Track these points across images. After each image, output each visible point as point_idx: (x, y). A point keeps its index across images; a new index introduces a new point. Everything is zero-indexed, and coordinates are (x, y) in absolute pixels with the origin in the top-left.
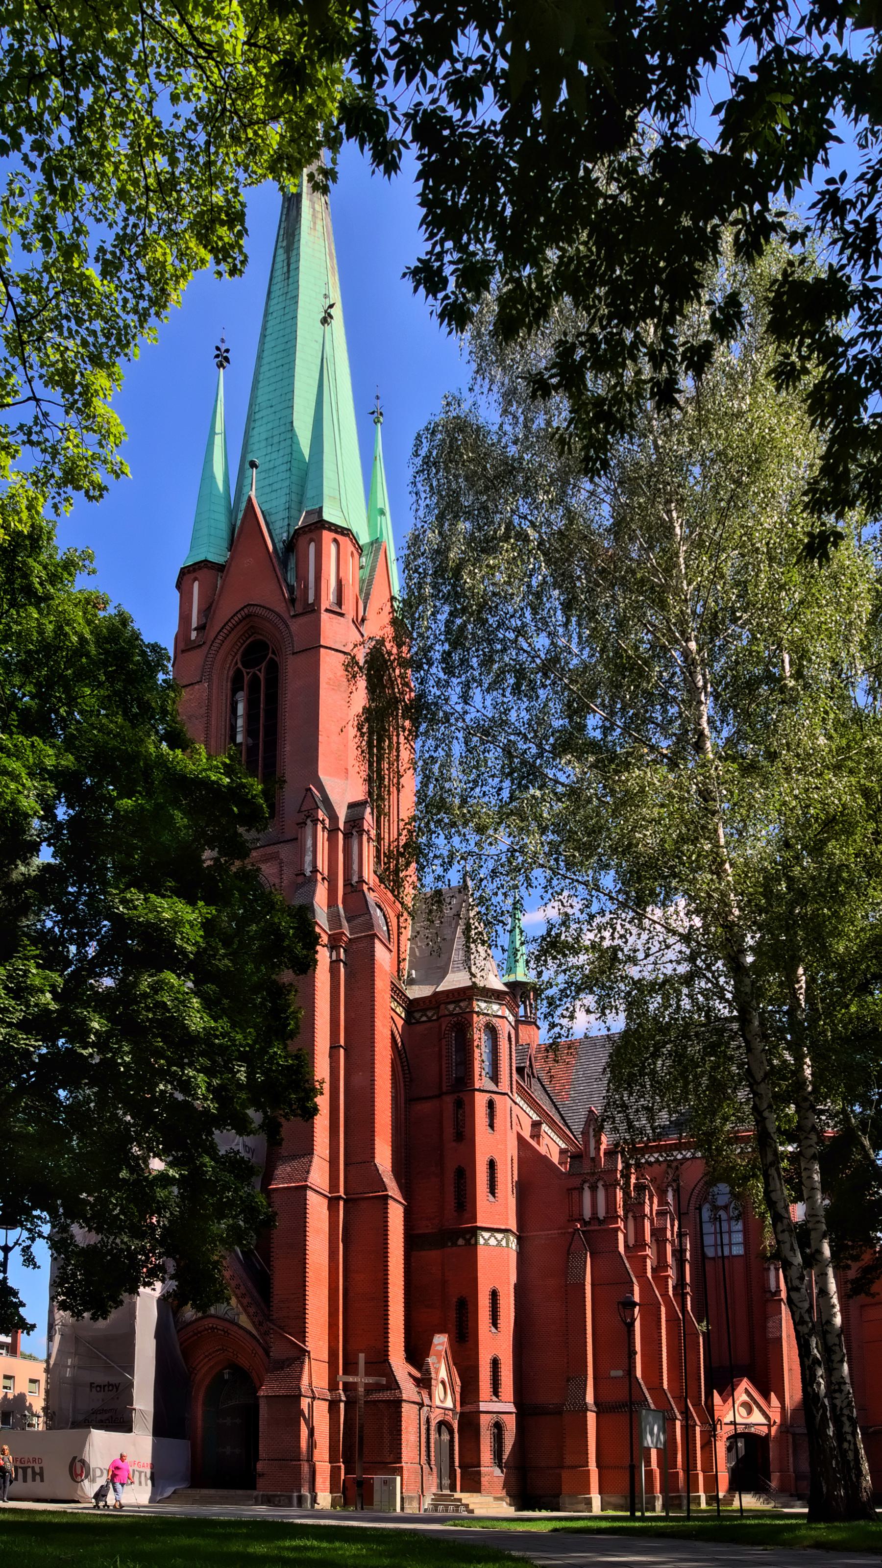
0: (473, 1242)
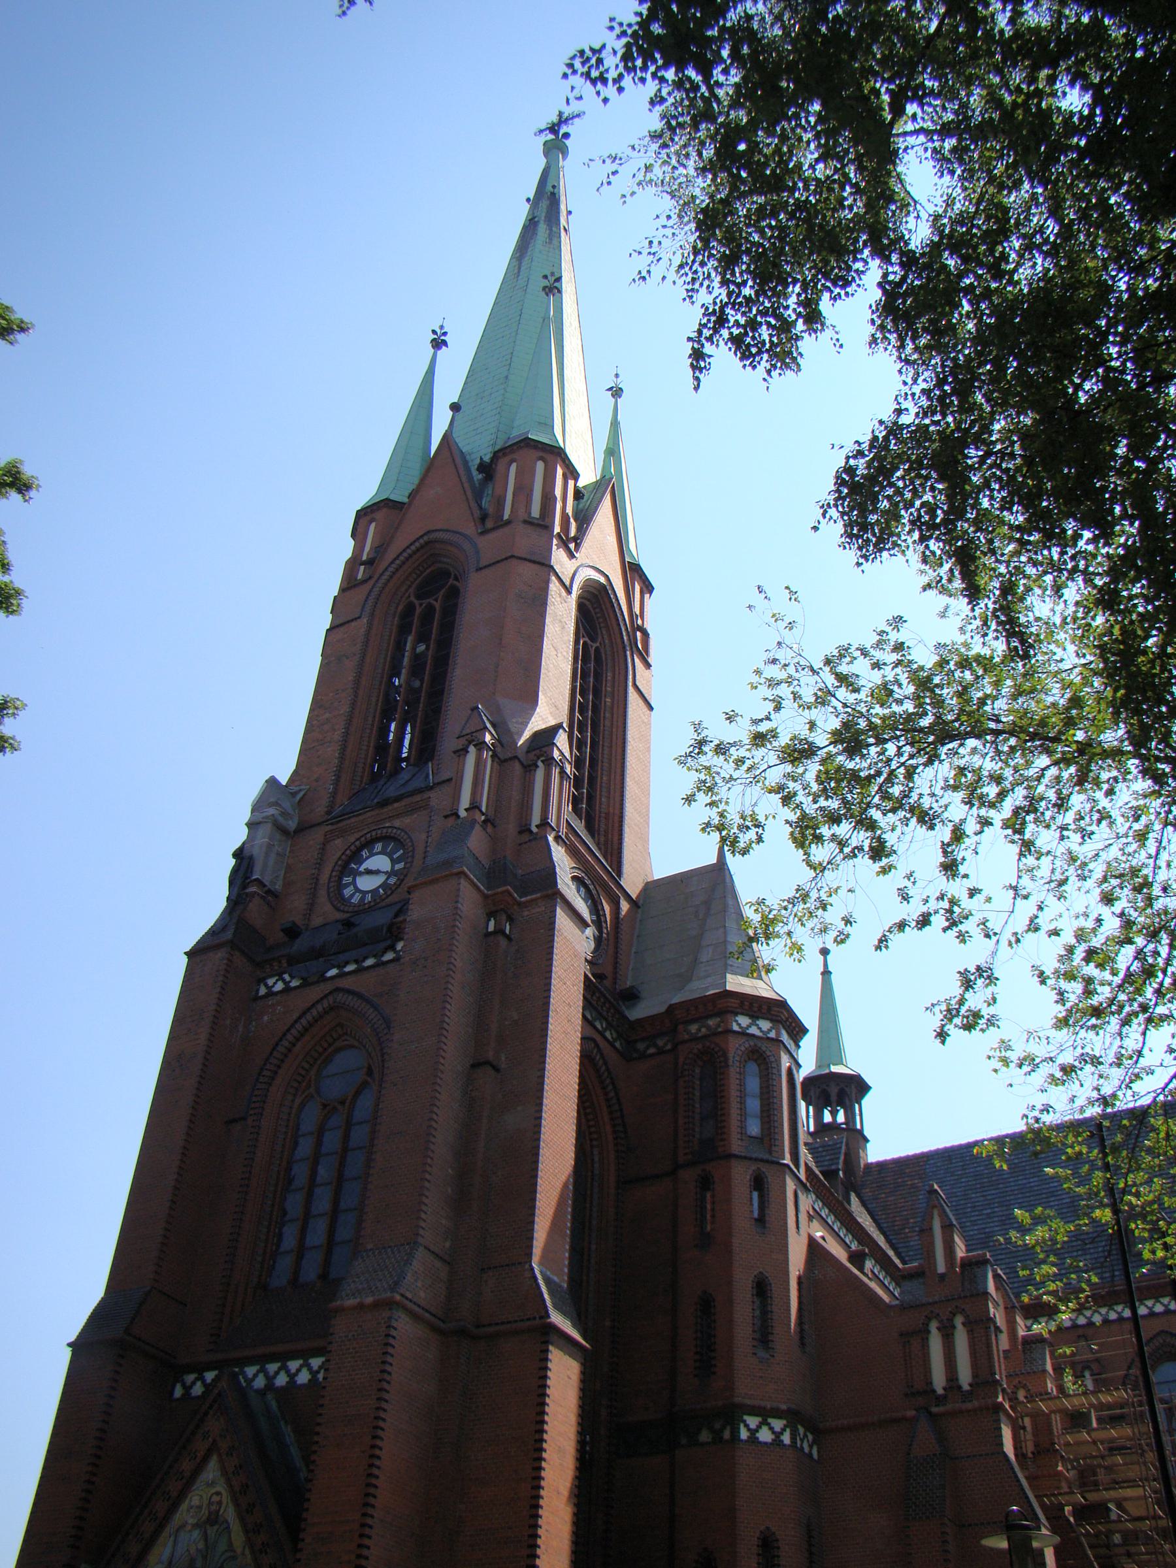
0: (727, 1434)
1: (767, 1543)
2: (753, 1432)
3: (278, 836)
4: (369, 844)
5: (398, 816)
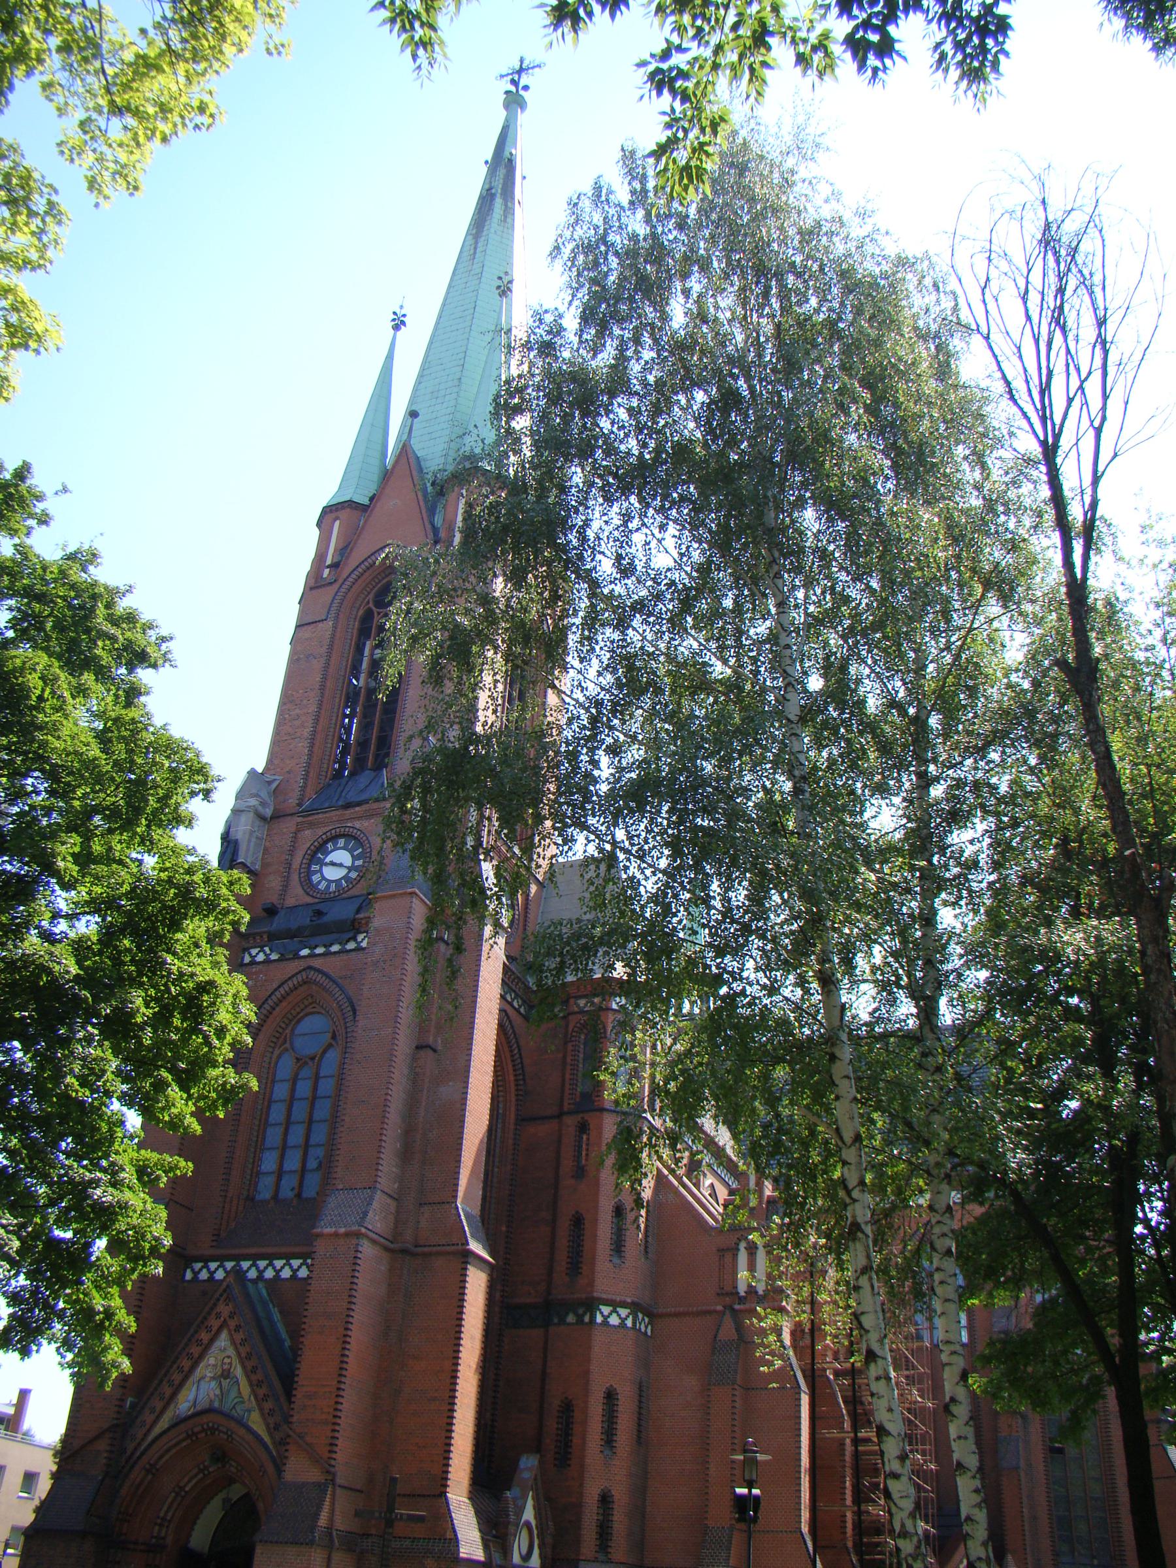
0: (587, 1319)
1: (610, 1396)
2: (606, 1318)
3: (258, 823)
4: (334, 839)
5: (359, 818)
